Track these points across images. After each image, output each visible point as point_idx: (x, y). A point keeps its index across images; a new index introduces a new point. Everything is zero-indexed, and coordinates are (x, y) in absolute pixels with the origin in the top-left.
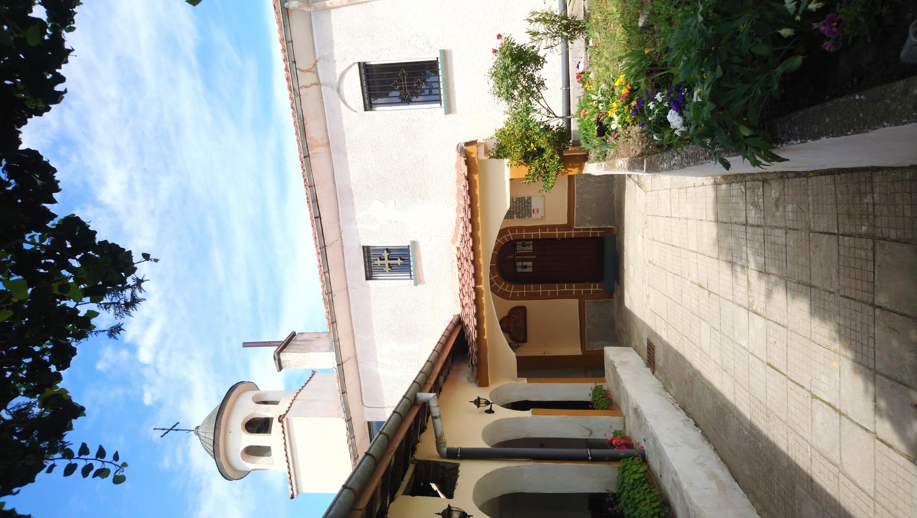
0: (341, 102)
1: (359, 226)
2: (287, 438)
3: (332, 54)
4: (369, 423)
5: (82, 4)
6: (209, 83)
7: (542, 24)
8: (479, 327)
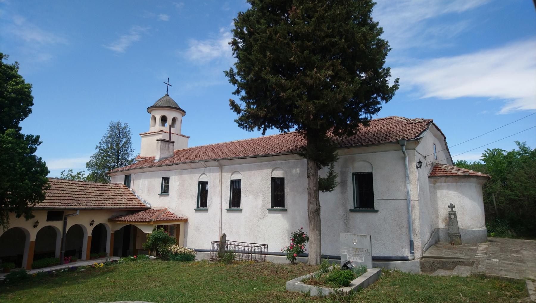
0: (200, 174)
1: (174, 176)
2: (156, 133)
3: (211, 173)
4: (131, 175)
5: (376, 3)
6: (430, 22)
7: (305, 233)
8: (118, 221)
